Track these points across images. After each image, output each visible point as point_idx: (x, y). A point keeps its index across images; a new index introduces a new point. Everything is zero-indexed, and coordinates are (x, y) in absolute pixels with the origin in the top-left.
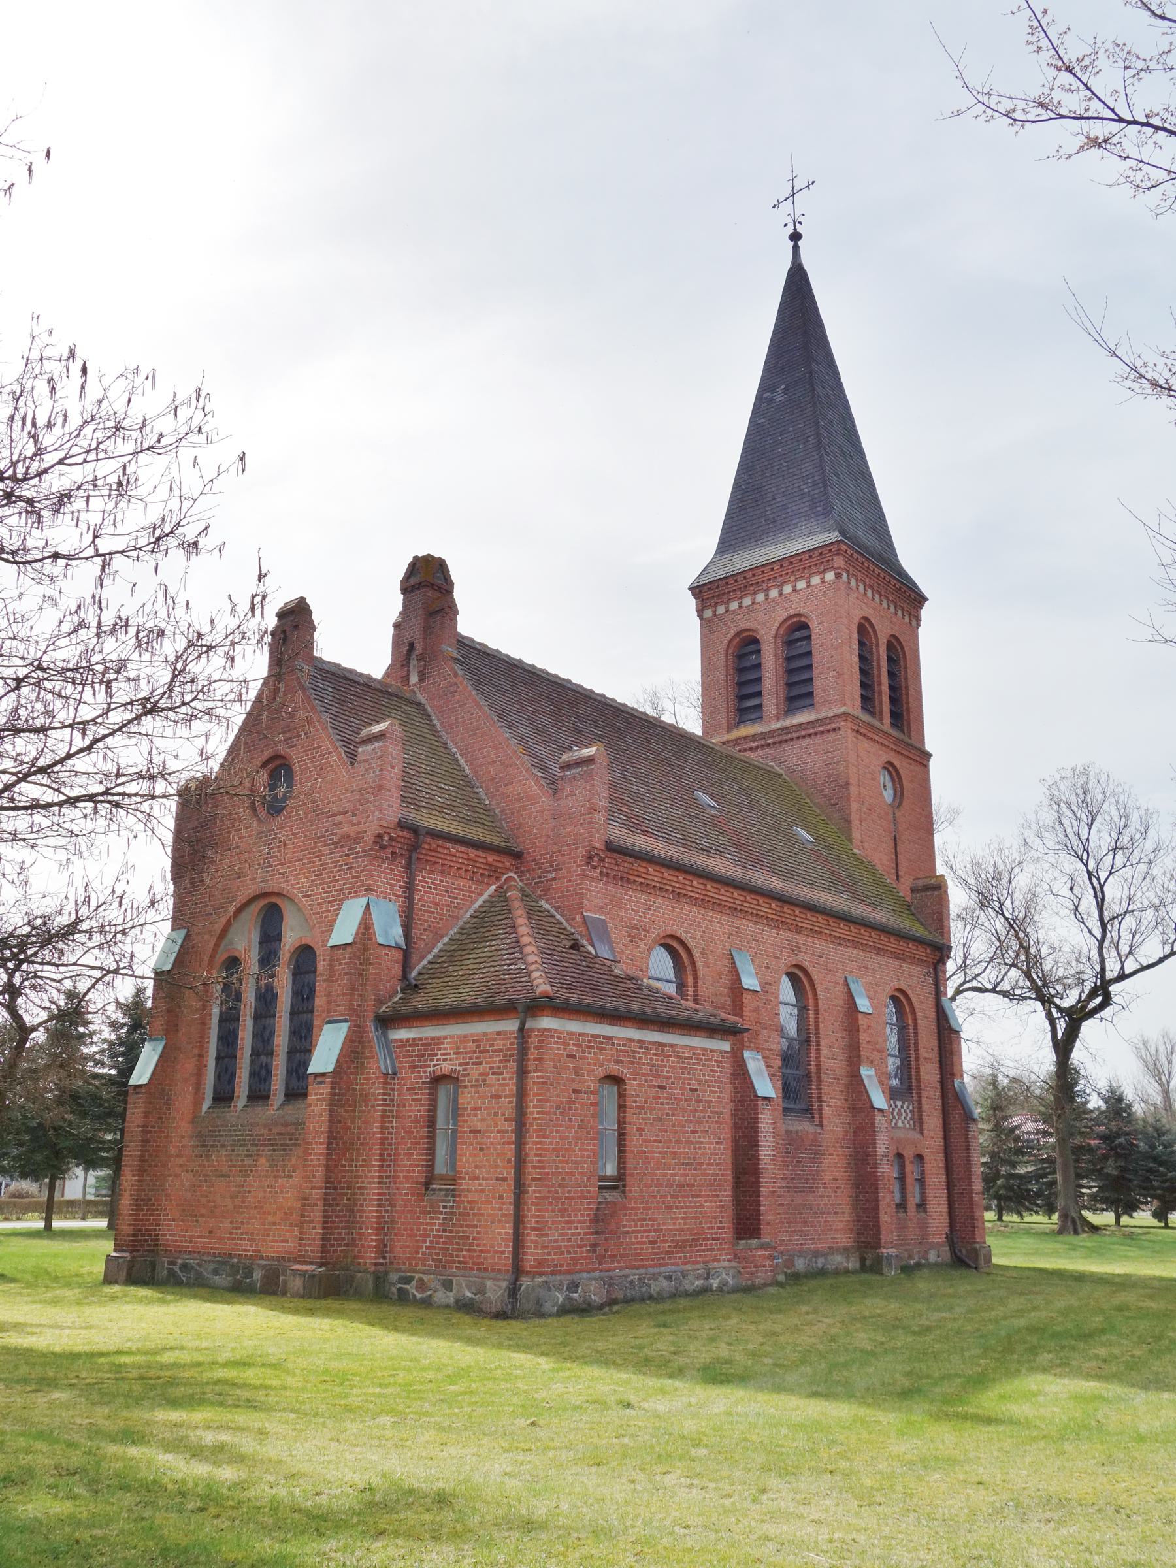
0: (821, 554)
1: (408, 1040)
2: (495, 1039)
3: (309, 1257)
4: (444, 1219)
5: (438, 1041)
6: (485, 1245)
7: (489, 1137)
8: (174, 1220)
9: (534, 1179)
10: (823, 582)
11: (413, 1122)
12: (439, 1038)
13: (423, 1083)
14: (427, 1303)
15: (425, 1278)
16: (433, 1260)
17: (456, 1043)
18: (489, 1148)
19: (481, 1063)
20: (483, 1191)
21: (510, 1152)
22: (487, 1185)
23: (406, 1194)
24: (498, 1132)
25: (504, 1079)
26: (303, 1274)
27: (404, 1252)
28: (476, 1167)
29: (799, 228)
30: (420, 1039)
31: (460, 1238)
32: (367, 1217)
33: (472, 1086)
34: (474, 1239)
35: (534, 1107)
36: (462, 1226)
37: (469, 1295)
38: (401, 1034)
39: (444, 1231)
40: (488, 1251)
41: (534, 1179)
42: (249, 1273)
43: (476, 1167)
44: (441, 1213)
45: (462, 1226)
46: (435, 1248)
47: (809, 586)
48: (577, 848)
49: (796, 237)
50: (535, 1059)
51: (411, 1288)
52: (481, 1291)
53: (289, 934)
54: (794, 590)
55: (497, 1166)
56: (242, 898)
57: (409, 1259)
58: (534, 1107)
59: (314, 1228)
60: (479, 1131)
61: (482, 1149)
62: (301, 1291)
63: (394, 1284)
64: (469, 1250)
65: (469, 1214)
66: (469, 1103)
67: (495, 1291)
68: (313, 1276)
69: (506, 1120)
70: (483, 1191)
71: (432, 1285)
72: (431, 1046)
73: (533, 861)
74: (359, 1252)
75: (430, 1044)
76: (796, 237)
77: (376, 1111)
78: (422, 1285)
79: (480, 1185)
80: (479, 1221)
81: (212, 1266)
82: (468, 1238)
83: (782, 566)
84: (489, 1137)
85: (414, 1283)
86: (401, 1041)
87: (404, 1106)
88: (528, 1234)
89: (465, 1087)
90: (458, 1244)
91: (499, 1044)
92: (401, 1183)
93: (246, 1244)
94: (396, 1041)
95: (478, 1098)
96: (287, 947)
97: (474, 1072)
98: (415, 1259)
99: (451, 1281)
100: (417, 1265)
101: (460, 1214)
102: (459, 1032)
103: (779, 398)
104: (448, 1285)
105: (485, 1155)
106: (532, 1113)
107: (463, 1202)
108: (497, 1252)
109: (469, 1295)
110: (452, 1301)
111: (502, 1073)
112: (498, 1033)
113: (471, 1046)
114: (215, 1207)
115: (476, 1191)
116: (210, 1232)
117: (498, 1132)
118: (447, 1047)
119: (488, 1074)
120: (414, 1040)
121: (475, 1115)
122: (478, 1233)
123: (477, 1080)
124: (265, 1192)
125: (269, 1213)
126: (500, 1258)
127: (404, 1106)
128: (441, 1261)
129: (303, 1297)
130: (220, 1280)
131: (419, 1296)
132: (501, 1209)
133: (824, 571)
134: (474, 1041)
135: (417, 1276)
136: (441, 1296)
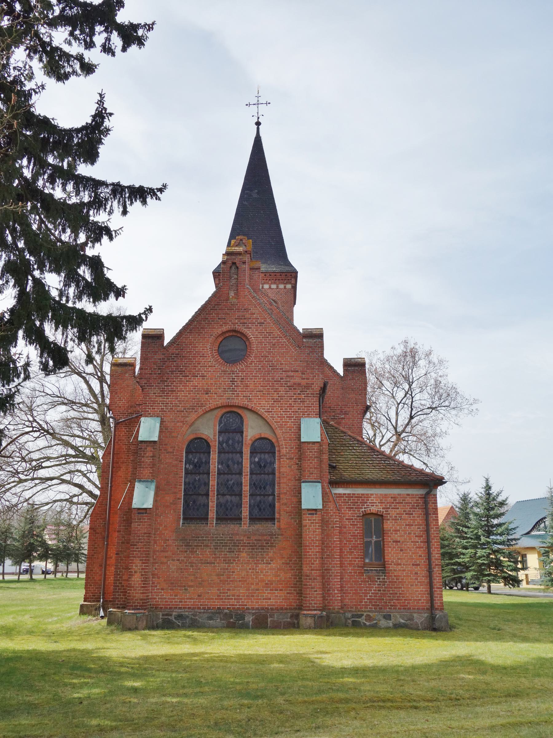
0: (286, 275)
1: (345, 494)
2: (406, 498)
3: (314, 607)
4: (378, 585)
5: (368, 496)
6: (407, 597)
7: (407, 545)
8: (162, 589)
9: (436, 565)
10: (285, 288)
11: (352, 536)
12: (367, 495)
13: (358, 516)
14: (375, 627)
15: (371, 614)
16: (373, 605)
17: (379, 498)
18: (406, 550)
19: (398, 508)
20: (404, 570)
21: (421, 552)
22: (407, 568)
23: (350, 573)
24: (412, 542)
25: (413, 517)
26: (314, 616)
27: (351, 602)
28: (399, 559)
29: (260, 120)
30: (354, 494)
31: (390, 594)
32: (334, 585)
33: (393, 519)
34: (400, 594)
35: (434, 531)
36: (391, 588)
37: (403, 621)
38: (340, 491)
39: (379, 590)
40: (411, 600)
41: (436, 565)
42: (242, 617)
43: (399, 559)
44: (377, 582)
45: (391, 588)
46: (373, 599)
47: (277, 288)
48: (357, 405)
49: (258, 124)
50: (433, 509)
51: (362, 620)
52: (411, 619)
53: (249, 430)
54: (270, 288)
55: (413, 559)
56: (207, 407)
57: (355, 605)
58: (434, 531)
59: (316, 591)
60: (399, 542)
61: (401, 550)
62: (313, 625)
63: (349, 619)
64: (397, 600)
65: (396, 582)
66: (391, 528)
67: (420, 618)
68: (322, 617)
69: (416, 536)
70: (404, 570)
71: (377, 618)
72: (363, 499)
73: (330, 407)
74: (329, 603)
75: (361, 497)
76: (258, 124)
77: (334, 530)
78: (369, 618)
79: (402, 567)
80: (403, 585)
81: (206, 615)
82: (396, 594)
83: (265, 275)
84: (407, 545)
85: (364, 617)
86: (339, 494)
87: (345, 528)
88: (435, 591)
89: (388, 520)
90: (389, 597)
91: (408, 499)
92: (345, 567)
93: (232, 602)
94: (335, 494)
95: (397, 525)
96: (249, 438)
97: (393, 513)
98: (359, 605)
99: (390, 615)
100: (361, 608)
101: (389, 582)
102: (382, 493)
103: (255, 195)
104: (387, 617)
105: (404, 553)
106: (434, 534)
107: (391, 576)
108: (416, 600)
109: (403, 621)
110: (391, 625)
111: (412, 514)
112: (408, 495)
113: (389, 500)
114: (202, 581)
115: (400, 570)
116: (199, 596)
117: (412, 542)
118: (373, 499)
119: (403, 514)
120: (349, 494)
121: (396, 534)
122: (403, 591)
123: (396, 517)
124: (248, 572)
125: (252, 584)
126: (418, 603)
127: (345, 528)
128: (378, 605)
129: (315, 628)
130: (218, 621)
131: (368, 623)
132: (417, 579)
133: (286, 284)
134: (392, 498)
135: (365, 614)
136: (383, 623)
